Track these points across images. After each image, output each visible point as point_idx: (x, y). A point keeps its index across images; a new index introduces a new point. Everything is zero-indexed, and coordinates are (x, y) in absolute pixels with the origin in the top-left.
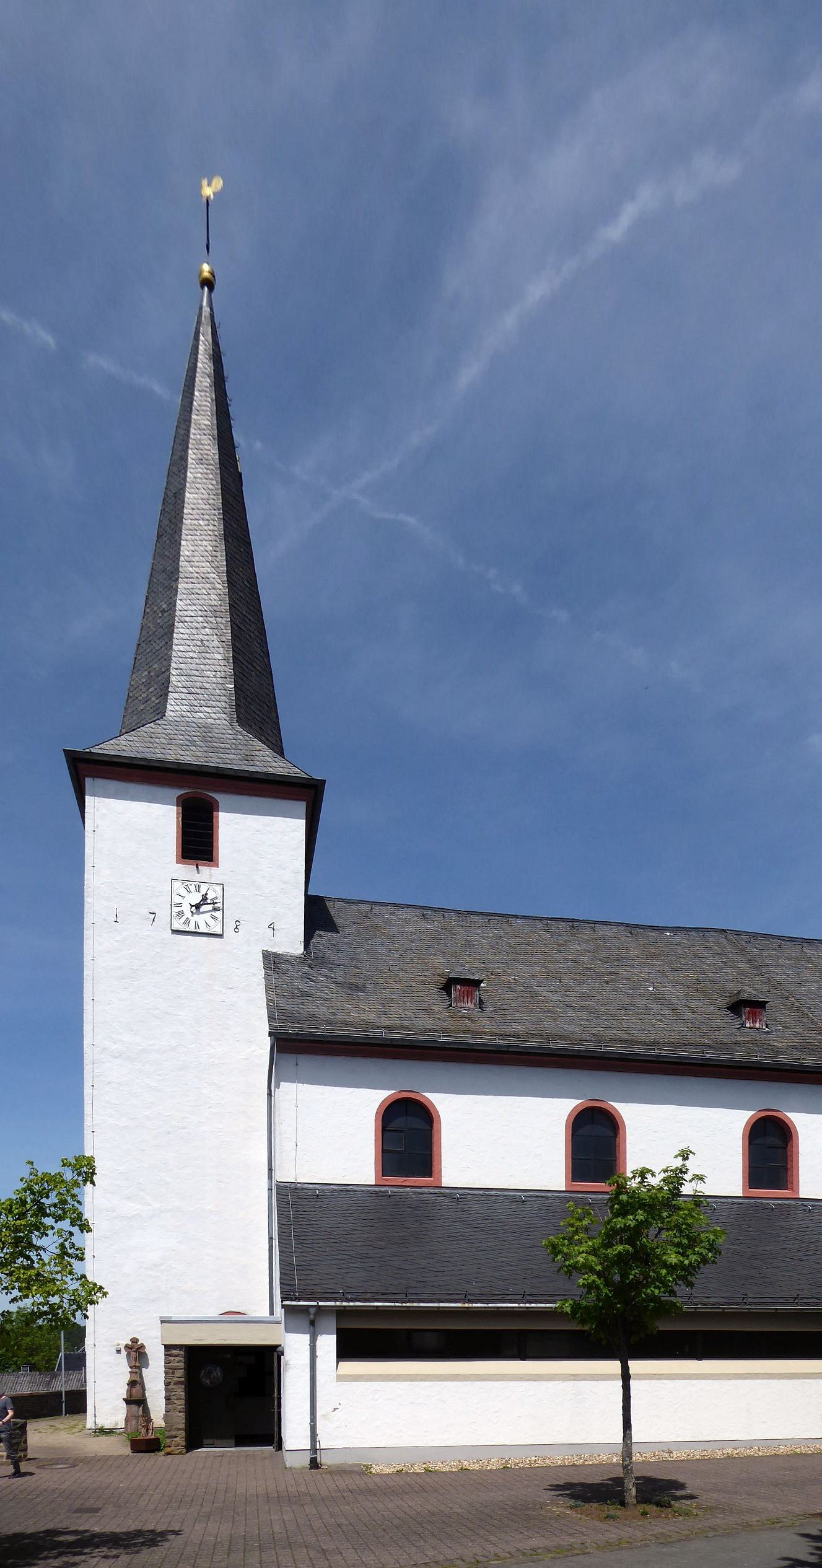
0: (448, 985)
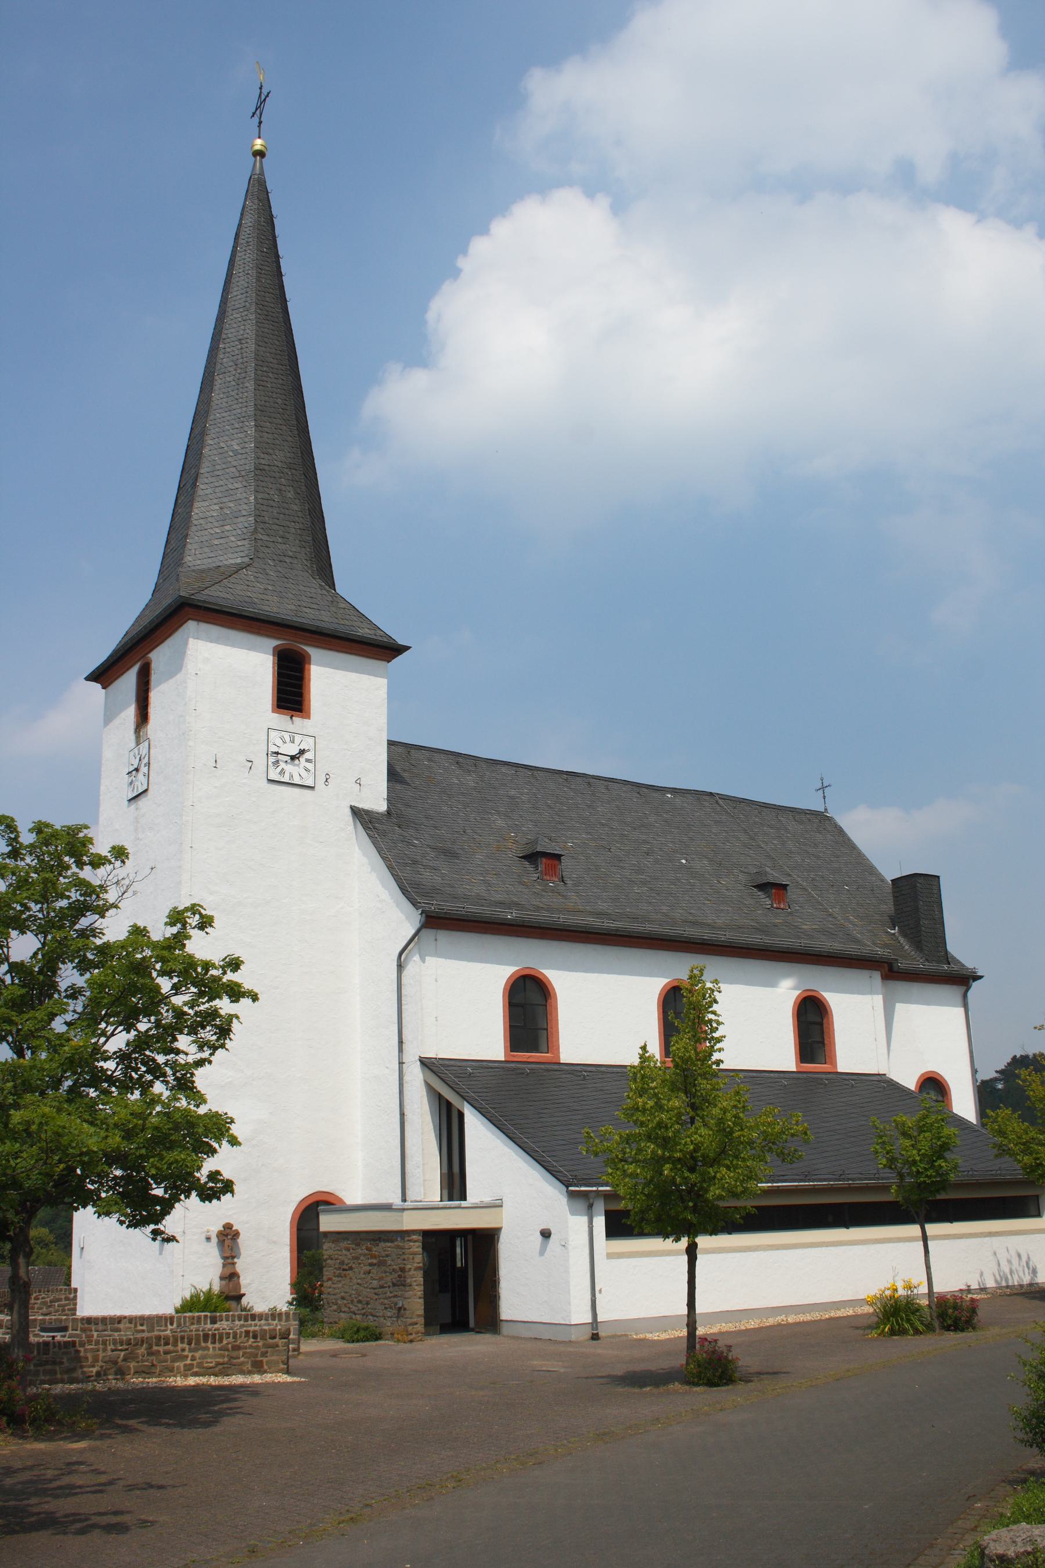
0: (532, 857)
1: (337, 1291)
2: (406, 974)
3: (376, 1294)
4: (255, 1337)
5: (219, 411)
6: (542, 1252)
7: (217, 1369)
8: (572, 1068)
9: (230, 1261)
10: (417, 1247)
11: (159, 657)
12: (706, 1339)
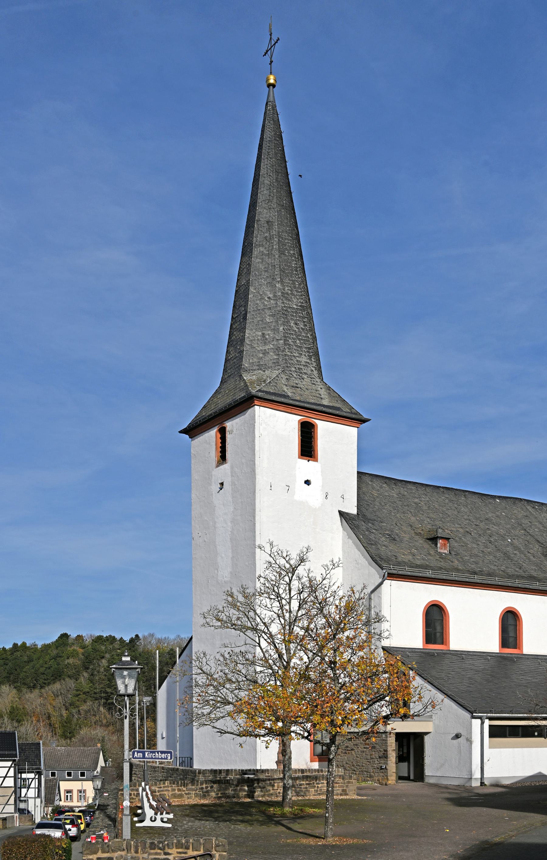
3: (368, 762)
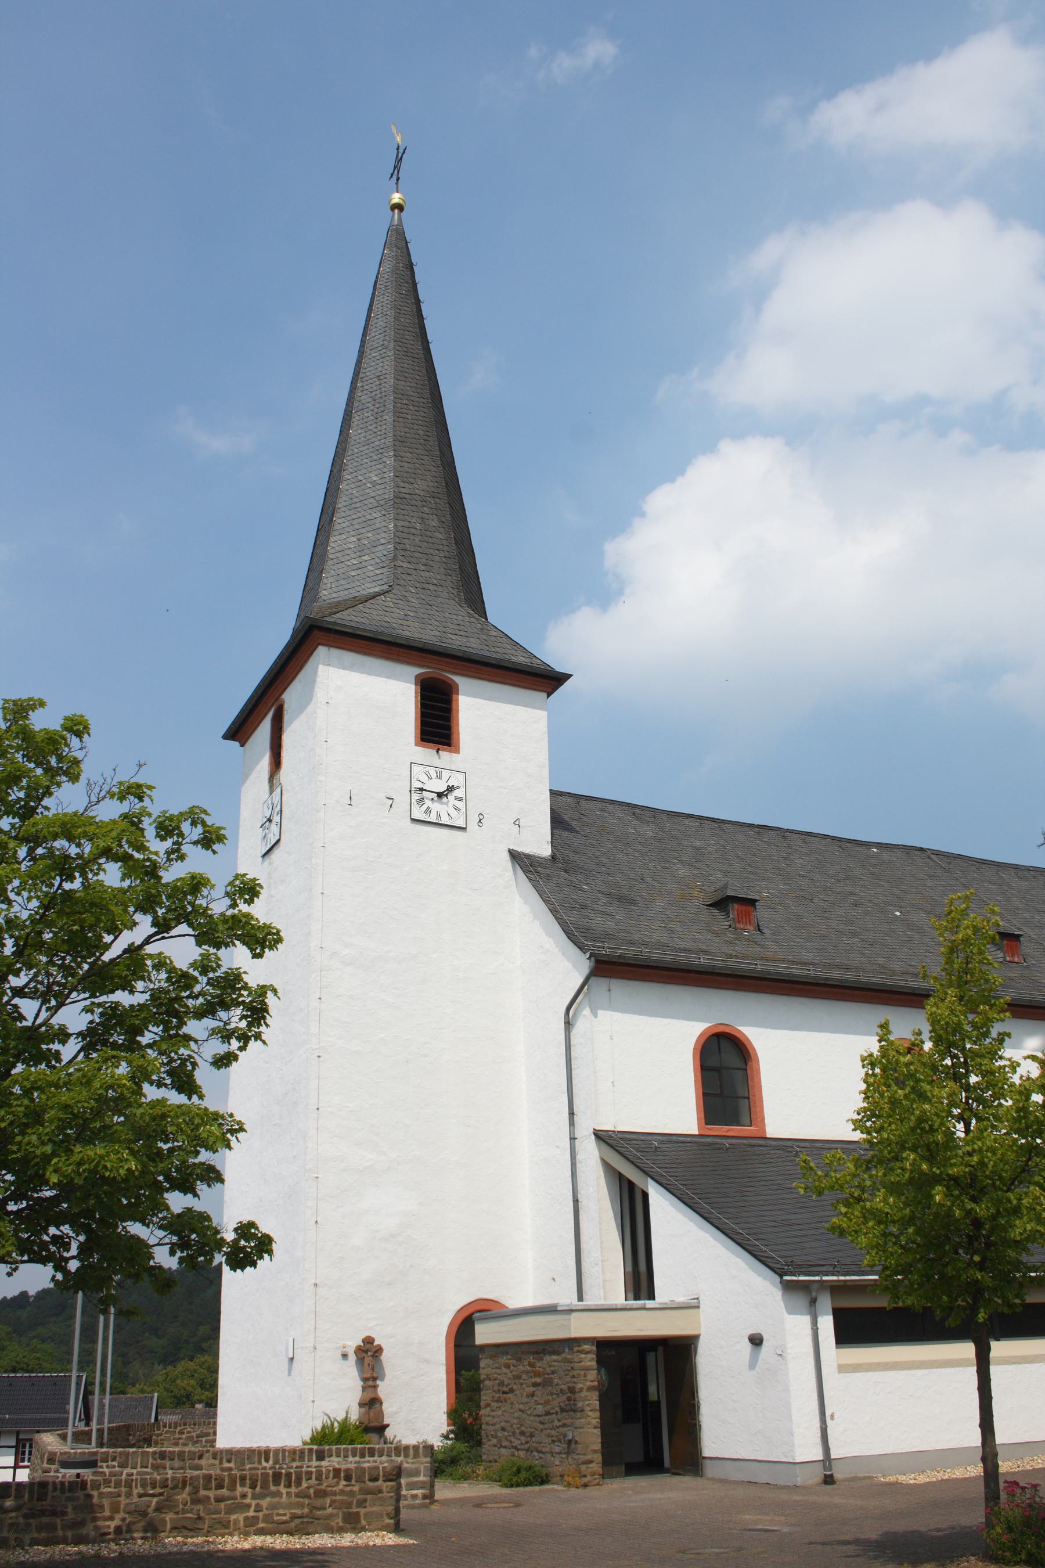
0: (722, 903)
1: (496, 1420)
2: (575, 1032)
3: (541, 1423)
4: (348, 1478)
5: (357, 446)
6: (752, 1364)
7: (293, 1524)
8: (782, 1143)
9: (371, 1383)
10: (589, 1360)
11: (291, 697)
12: (1016, 1483)
